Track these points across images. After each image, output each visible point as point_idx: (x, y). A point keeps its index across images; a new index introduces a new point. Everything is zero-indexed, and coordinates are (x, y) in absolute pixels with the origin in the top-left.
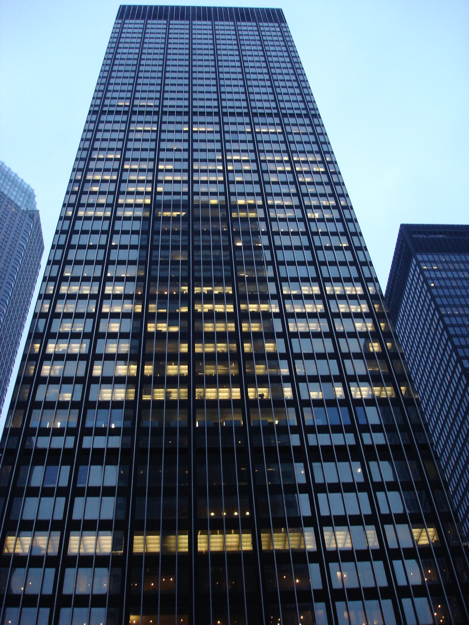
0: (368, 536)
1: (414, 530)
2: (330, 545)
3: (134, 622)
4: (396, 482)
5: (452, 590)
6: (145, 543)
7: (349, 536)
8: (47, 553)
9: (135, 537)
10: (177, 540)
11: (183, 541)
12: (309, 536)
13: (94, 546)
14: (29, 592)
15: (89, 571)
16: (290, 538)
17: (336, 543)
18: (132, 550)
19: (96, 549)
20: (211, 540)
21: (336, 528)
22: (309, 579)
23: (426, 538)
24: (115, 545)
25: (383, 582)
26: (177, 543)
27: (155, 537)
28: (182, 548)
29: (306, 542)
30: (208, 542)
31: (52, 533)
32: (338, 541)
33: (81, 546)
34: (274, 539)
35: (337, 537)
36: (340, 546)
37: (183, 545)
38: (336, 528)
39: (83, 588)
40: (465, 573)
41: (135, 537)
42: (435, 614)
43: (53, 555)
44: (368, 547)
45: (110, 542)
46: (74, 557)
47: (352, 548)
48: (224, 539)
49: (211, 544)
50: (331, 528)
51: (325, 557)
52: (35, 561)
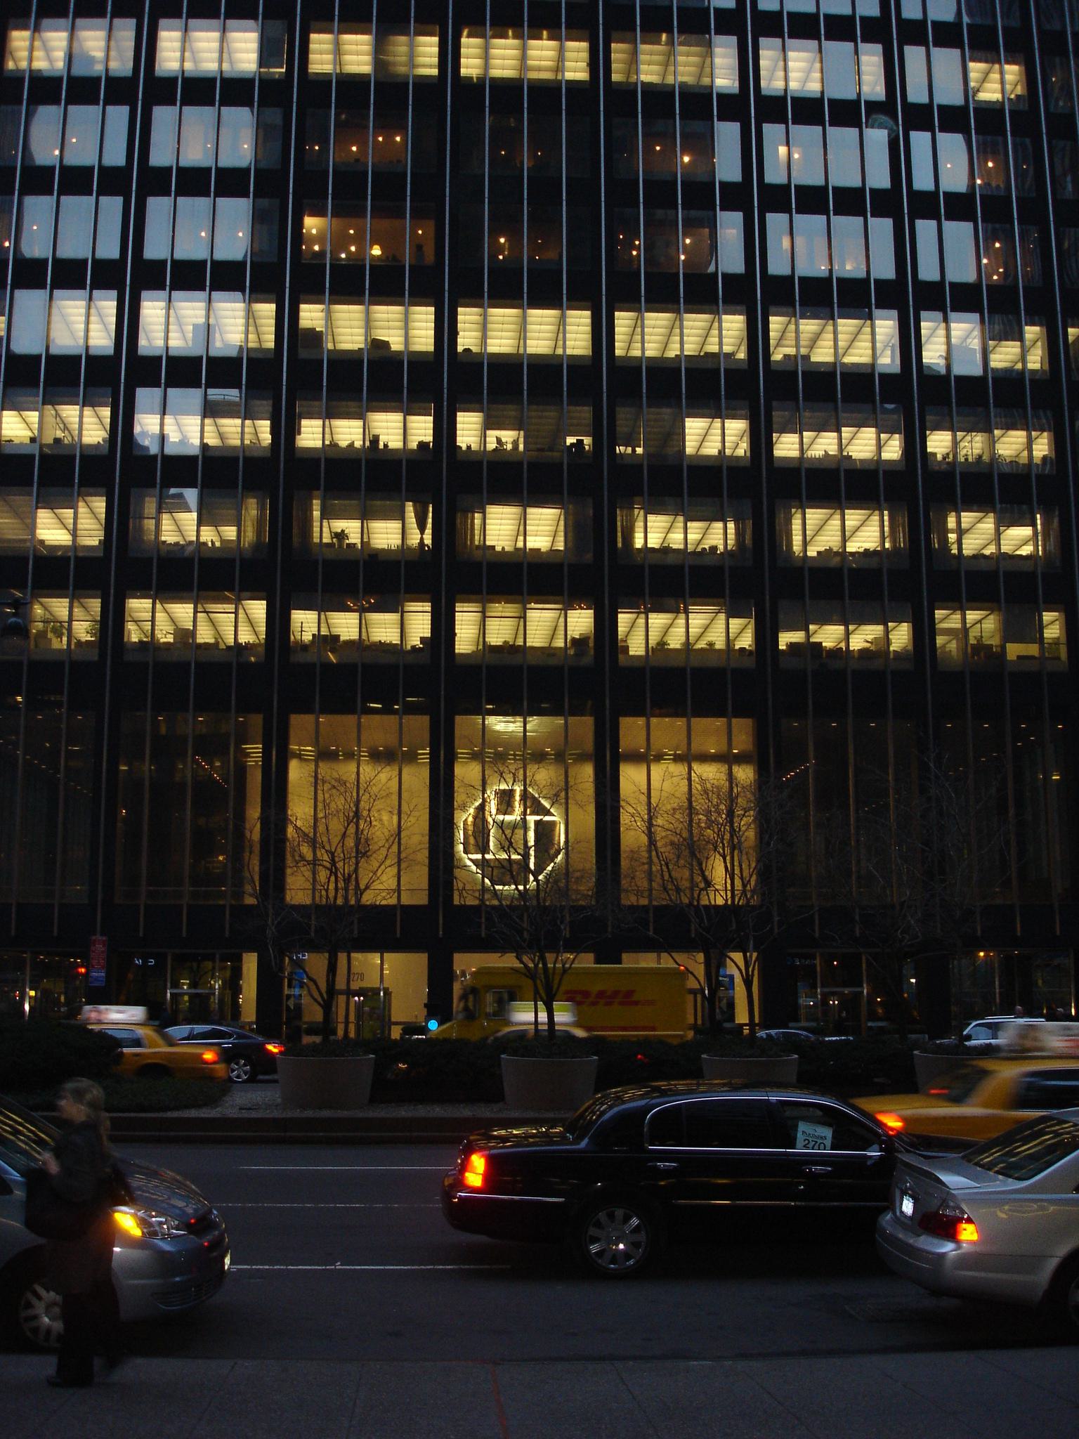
0: (863, 68)
1: (971, 65)
2: (772, 83)
3: (314, 231)
4: (957, 25)
5: (1033, 212)
6: (338, 51)
7: (818, 65)
8: (107, 70)
9: (313, 36)
10: (412, 46)
11: (427, 50)
12: (724, 56)
13: (216, 55)
14: (72, 160)
15: (208, 112)
16: (680, 59)
17: (786, 79)
18: (307, 68)
19: (221, 61)
20: (493, 52)
21: (789, 42)
22: (713, 157)
23: (998, 86)
24: (266, 55)
25: (880, 178)
26: (412, 55)
27: (359, 37)
28: (424, 66)
29: (717, 71)
30: (486, 57)
31: (117, 21)
32: (791, 75)
33: (187, 54)
34: (642, 57)
35: (791, 64)
36: (793, 85)
37: (427, 60)
38: (790, 42)
39: (196, 154)
40: (1069, 178)
41: (313, 36)
42: (985, 261)
43: (123, 74)
44: (859, 95)
45: (254, 46)
46: (170, 82)
47: (822, 93)
48: (524, 49)
49: (493, 62)
50: (778, 41)
51: (756, 108)
52: (81, 89)
